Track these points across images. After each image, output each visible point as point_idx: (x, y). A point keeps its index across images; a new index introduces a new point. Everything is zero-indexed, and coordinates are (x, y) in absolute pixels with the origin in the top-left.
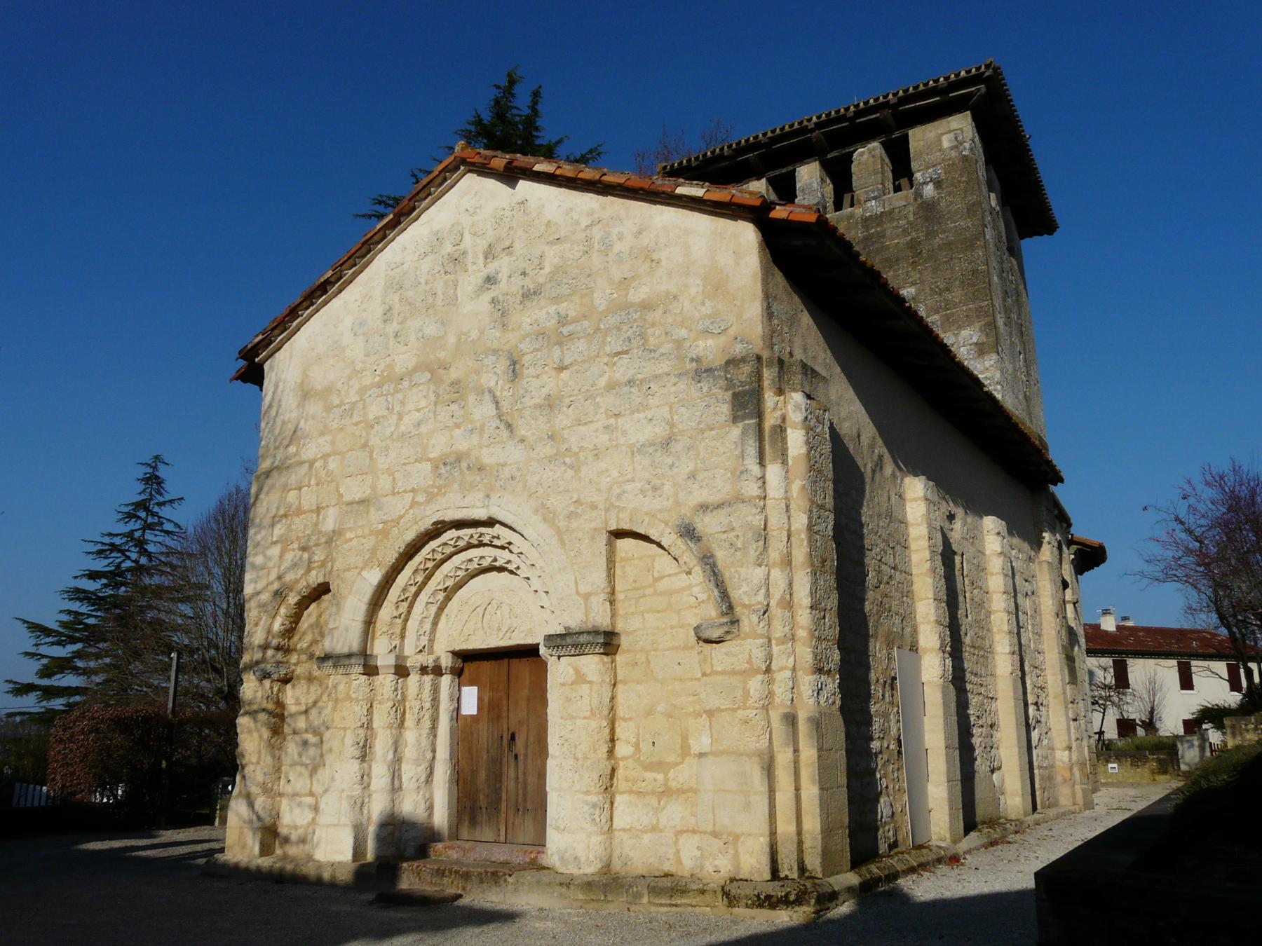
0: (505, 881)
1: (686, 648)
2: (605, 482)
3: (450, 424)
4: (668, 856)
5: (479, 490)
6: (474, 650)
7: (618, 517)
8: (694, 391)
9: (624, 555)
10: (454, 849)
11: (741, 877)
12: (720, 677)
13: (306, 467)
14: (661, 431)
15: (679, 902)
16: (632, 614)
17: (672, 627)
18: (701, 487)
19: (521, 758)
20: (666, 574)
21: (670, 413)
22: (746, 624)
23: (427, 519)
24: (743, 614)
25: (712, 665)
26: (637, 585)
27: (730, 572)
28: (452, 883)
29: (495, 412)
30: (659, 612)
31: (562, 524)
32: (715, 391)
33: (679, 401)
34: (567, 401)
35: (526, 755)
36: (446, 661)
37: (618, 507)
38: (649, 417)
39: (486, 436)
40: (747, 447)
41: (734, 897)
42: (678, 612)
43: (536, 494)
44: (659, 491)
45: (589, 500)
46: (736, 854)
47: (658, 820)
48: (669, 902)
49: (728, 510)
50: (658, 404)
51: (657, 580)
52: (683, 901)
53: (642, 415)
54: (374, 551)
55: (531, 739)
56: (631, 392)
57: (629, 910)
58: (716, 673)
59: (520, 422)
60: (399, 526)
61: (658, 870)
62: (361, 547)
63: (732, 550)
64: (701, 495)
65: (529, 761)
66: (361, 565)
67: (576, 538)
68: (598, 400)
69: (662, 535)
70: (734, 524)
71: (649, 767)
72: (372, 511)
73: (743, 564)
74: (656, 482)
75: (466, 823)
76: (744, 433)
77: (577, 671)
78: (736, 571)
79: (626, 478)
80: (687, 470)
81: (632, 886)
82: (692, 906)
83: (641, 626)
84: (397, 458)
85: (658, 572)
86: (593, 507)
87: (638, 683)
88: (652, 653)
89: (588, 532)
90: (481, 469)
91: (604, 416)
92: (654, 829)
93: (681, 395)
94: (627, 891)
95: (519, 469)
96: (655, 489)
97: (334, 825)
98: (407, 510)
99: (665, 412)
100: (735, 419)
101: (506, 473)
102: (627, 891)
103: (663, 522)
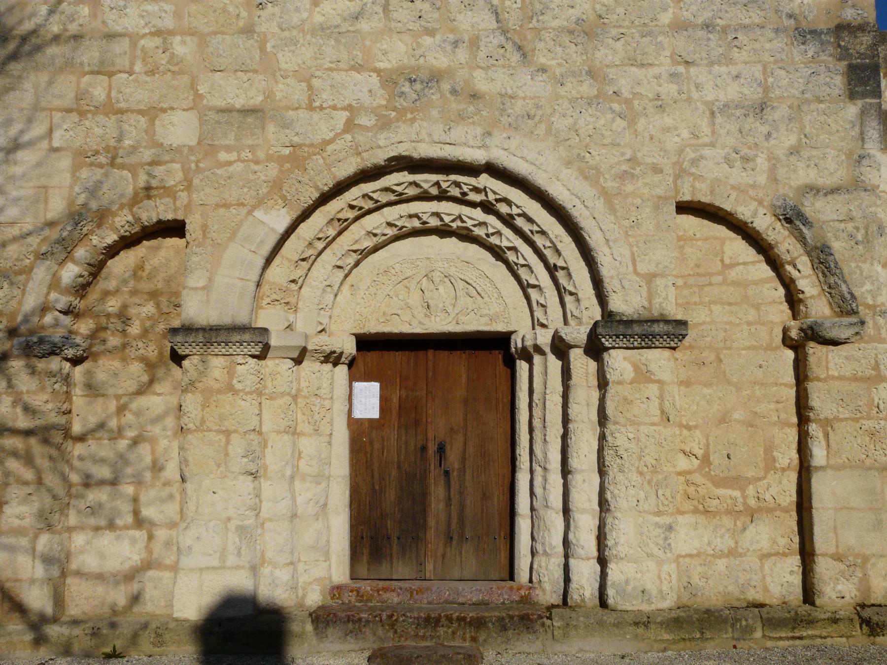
0: (543, 625)
1: (770, 348)
2: (672, 142)
3: (415, 26)
4: (753, 583)
5: (474, 123)
6: (401, 334)
7: (693, 186)
8: (799, 54)
9: (681, 234)
10: (393, 591)
11: (872, 602)
12: (837, 383)
13: (125, 43)
14: (753, 93)
15: (805, 634)
16: (695, 303)
17: (749, 324)
18: (808, 166)
19: (455, 475)
20: (741, 261)
21: (764, 74)
22: (871, 326)
23: (379, 151)
24: (867, 314)
25: (827, 369)
26: (701, 270)
27: (850, 266)
28: (454, 633)
29: (494, 25)
30: (730, 304)
31: (611, 185)
32: (823, 57)
33: (776, 62)
34: (614, 32)
35: (462, 471)
36: (350, 347)
37: (693, 174)
38: (734, 73)
39: (482, 55)
40: (868, 129)
41: (877, 624)
42: (757, 307)
43: (568, 143)
44: (751, 163)
45: (649, 160)
46: (865, 578)
47: (736, 543)
48: (791, 634)
49: (847, 196)
50: (747, 60)
51: (726, 267)
52: (810, 632)
53: (724, 69)
54: (277, 185)
55: (471, 450)
56: (709, 39)
57: (735, 647)
58: (833, 378)
59: (540, 45)
60: (325, 155)
61: (738, 600)
62: (252, 177)
63: (853, 243)
64: (804, 175)
65: (468, 477)
66: (253, 202)
67: (633, 204)
68: (659, 39)
69: (755, 214)
70: (854, 214)
71: (720, 482)
72: (271, 128)
73: (866, 259)
74: (745, 151)
75: (365, 558)
76: (863, 113)
77: (636, 368)
78: (857, 266)
79: (700, 141)
80: (788, 144)
81: (740, 620)
82: (821, 637)
83: (708, 319)
84: (316, 59)
85: (731, 258)
86: (657, 170)
87: (705, 386)
88: (724, 352)
89: (648, 200)
90: (475, 96)
91: (668, 60)
92: (731, 553)
93: (778, 55)
94: (733, 626)
95: (538, 107)
96: (746, 159)
97: (214, 568)
98: (337, 135)
99: (757, 70)
100: (852, 96)
101: (519, 107)
102: (733, 626)
103: (755, 200)
